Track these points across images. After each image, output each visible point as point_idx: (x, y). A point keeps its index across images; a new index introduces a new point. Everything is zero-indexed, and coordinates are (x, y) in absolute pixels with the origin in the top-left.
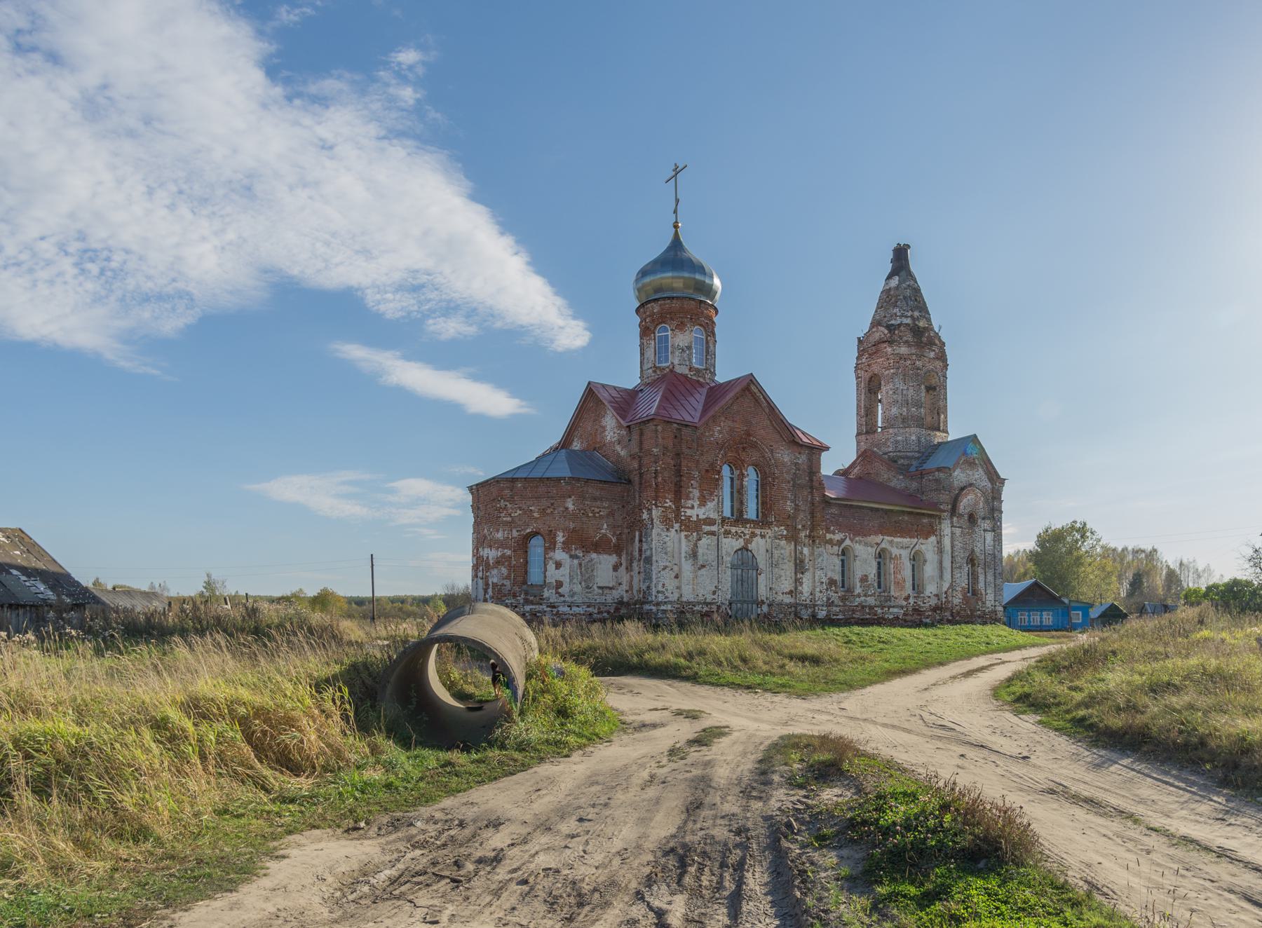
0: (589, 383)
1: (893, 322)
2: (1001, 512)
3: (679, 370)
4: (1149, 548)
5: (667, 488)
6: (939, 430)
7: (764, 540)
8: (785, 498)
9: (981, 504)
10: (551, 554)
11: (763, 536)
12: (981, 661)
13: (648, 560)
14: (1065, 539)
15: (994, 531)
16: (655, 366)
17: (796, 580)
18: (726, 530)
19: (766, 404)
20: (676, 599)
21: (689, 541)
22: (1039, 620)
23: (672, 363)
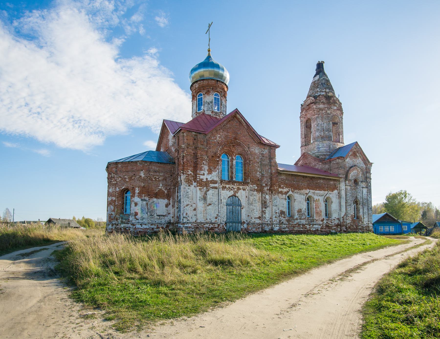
0: (164, 120)
1: (316, 94)
2: (371, 179)
3: (207, 113)
4: (428, 202)
5: (189, 164)
6: (339, 142)
7: (245, 192)
8: (257, 171)
9: (360, 175)
10: (133, 199)
11: (244, 190)
12: (358, 259)
13: (179, 202)
14: (397, 197)
15: (367, 188)
16: (196, 112)
17: (262, 211)
18: (223, 187)
19: (245, 124)
20: (194, 221)
21: (202, 191)
22: (388, 229)
23: (204, 110)
